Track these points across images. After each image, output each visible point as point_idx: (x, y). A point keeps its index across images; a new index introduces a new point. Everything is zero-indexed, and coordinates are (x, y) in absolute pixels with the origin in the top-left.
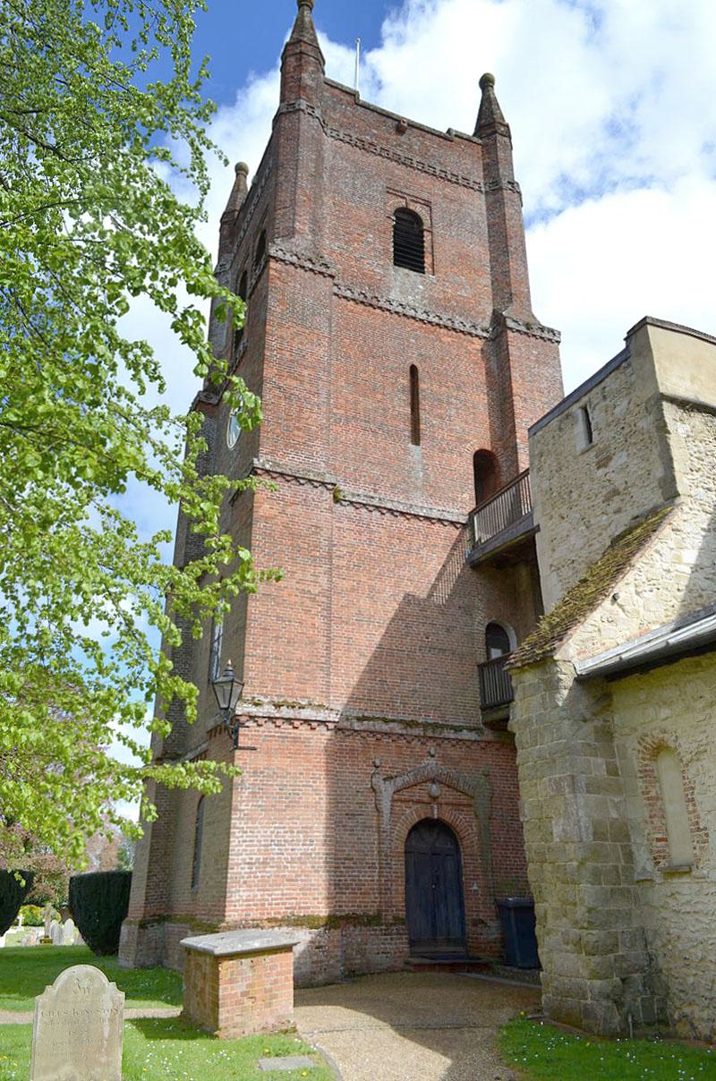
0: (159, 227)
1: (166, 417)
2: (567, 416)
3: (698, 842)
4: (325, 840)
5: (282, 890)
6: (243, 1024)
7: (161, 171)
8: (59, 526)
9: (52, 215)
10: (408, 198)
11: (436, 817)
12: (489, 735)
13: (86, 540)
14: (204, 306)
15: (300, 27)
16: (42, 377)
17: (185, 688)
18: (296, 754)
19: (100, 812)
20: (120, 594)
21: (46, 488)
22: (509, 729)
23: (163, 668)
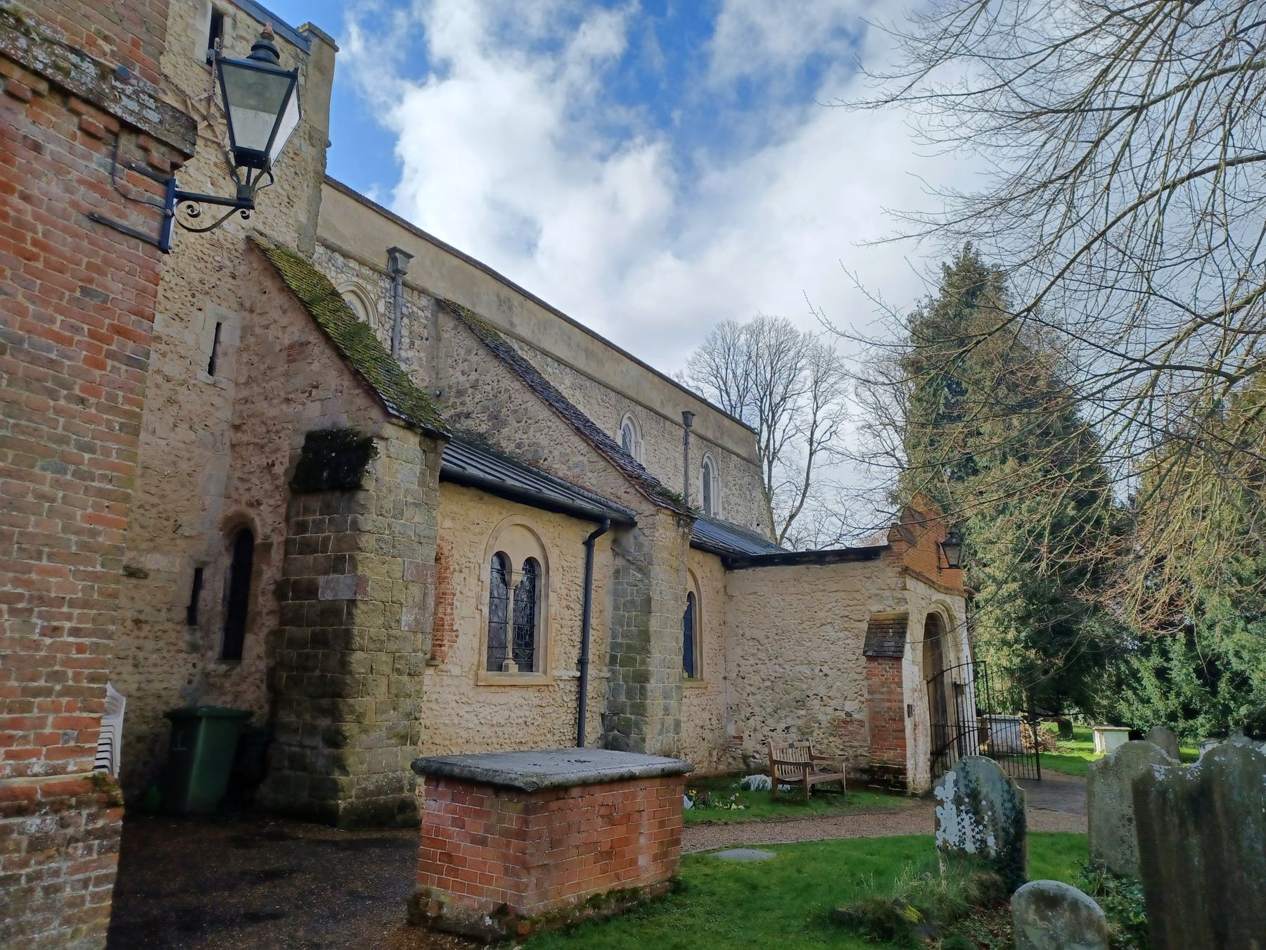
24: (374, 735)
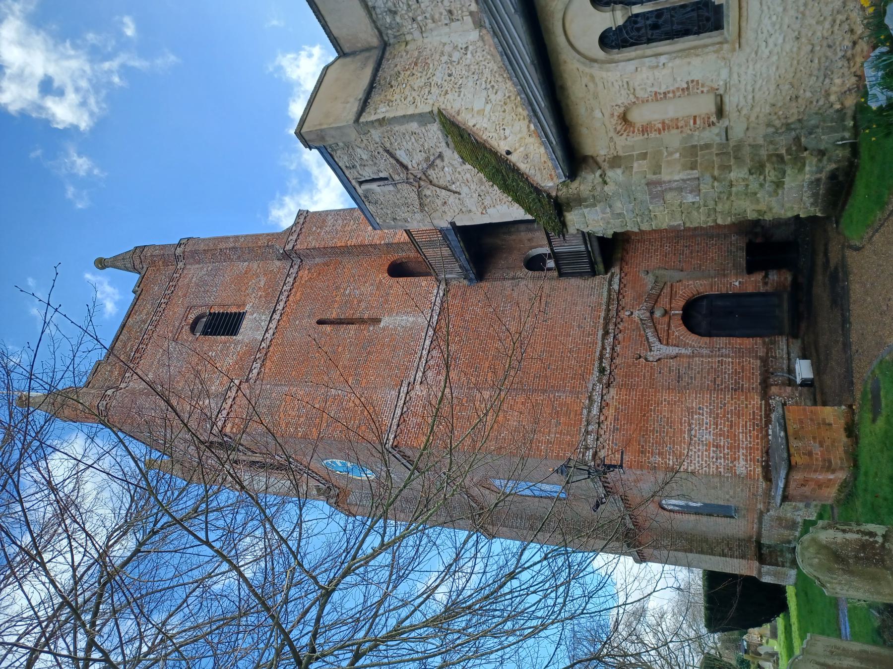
2: (366, 197)
3: (698, 89)
5: (739, 433)
11: (681, 312)
24: (774, 204)
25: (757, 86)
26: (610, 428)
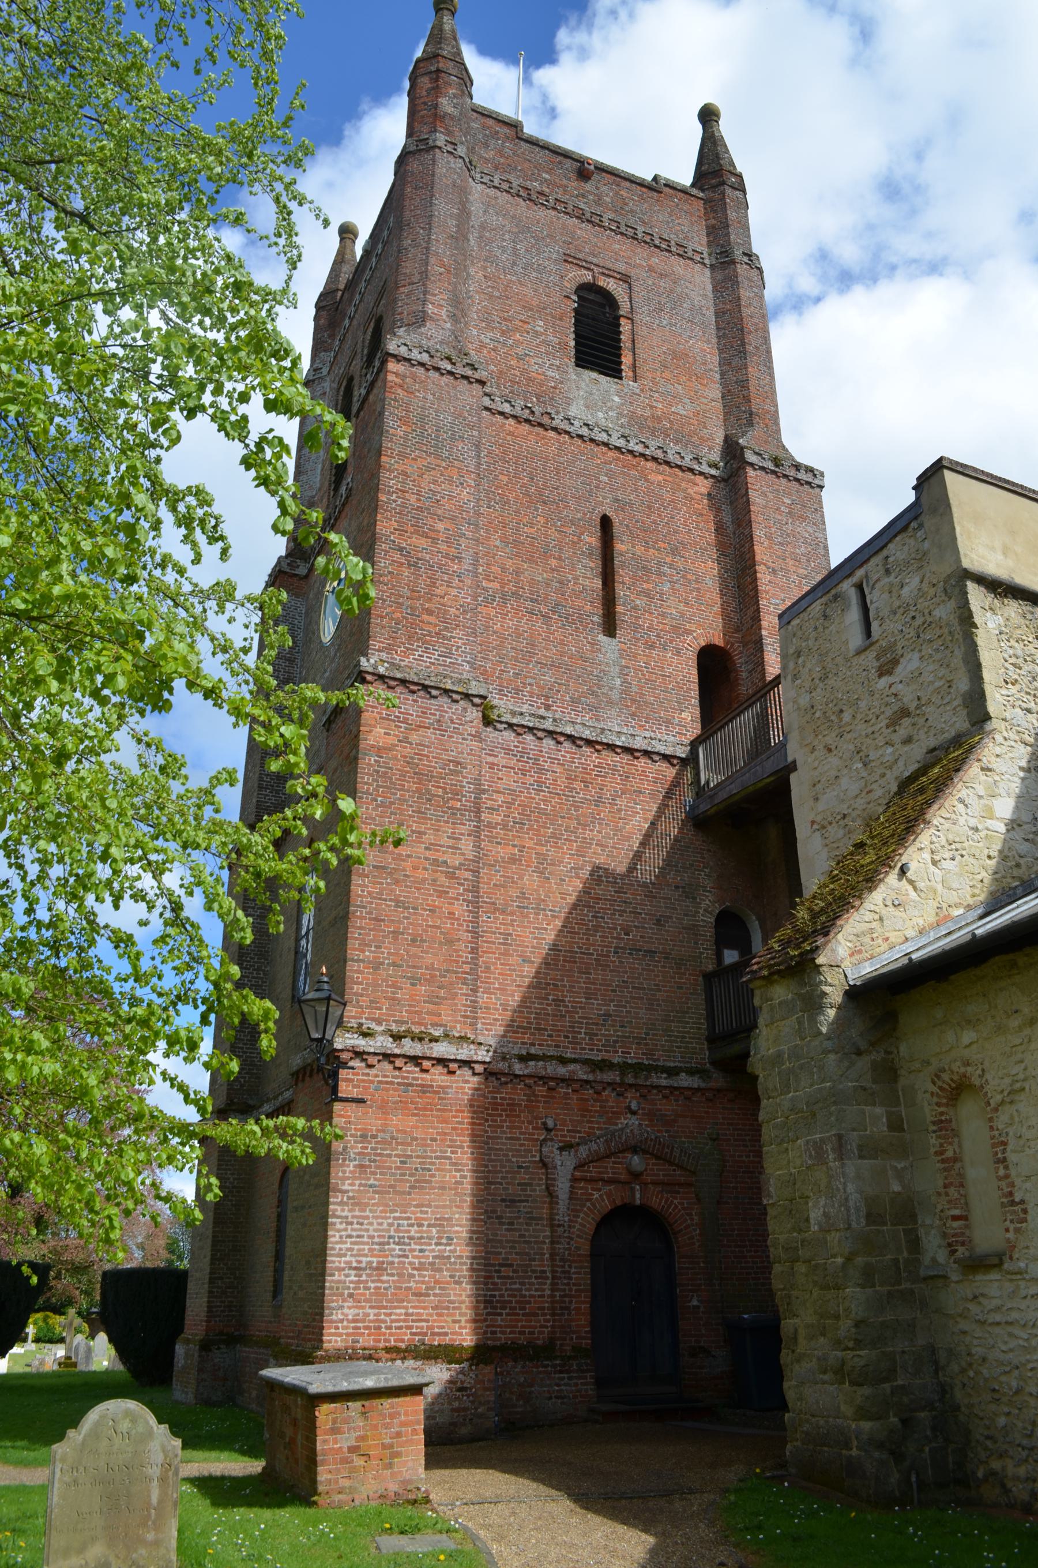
0: (226, 318)
1: (230, 596)
4: (471, 1238)
5: (406, 1308)
6: (352, 1490)
7: (231, 240)
8: (79, 761)
9: (79, 311)
10: (596, 269)
11: (638, 1202)
12: (718, 1080)
13: (115, 783)
14: (288, 429)
15: (437, 37)
16: (60, 545)
17: (258, 1007)
18: (425, 1109)
19: (142, 1181)
20: (164, 863)
21: (62, 705)
22: (749, 1070)
23: (227, 976)
25: (1017, 1331)
26: (407, 1078)
